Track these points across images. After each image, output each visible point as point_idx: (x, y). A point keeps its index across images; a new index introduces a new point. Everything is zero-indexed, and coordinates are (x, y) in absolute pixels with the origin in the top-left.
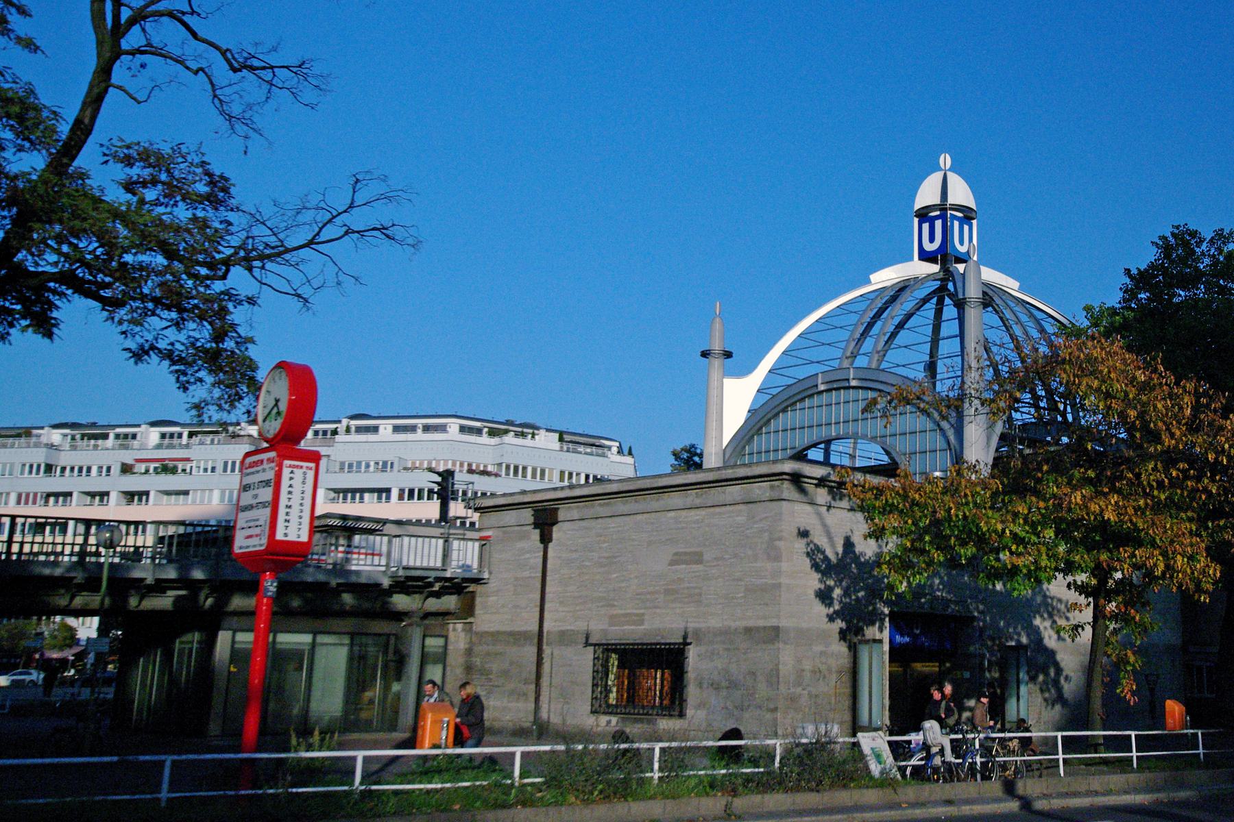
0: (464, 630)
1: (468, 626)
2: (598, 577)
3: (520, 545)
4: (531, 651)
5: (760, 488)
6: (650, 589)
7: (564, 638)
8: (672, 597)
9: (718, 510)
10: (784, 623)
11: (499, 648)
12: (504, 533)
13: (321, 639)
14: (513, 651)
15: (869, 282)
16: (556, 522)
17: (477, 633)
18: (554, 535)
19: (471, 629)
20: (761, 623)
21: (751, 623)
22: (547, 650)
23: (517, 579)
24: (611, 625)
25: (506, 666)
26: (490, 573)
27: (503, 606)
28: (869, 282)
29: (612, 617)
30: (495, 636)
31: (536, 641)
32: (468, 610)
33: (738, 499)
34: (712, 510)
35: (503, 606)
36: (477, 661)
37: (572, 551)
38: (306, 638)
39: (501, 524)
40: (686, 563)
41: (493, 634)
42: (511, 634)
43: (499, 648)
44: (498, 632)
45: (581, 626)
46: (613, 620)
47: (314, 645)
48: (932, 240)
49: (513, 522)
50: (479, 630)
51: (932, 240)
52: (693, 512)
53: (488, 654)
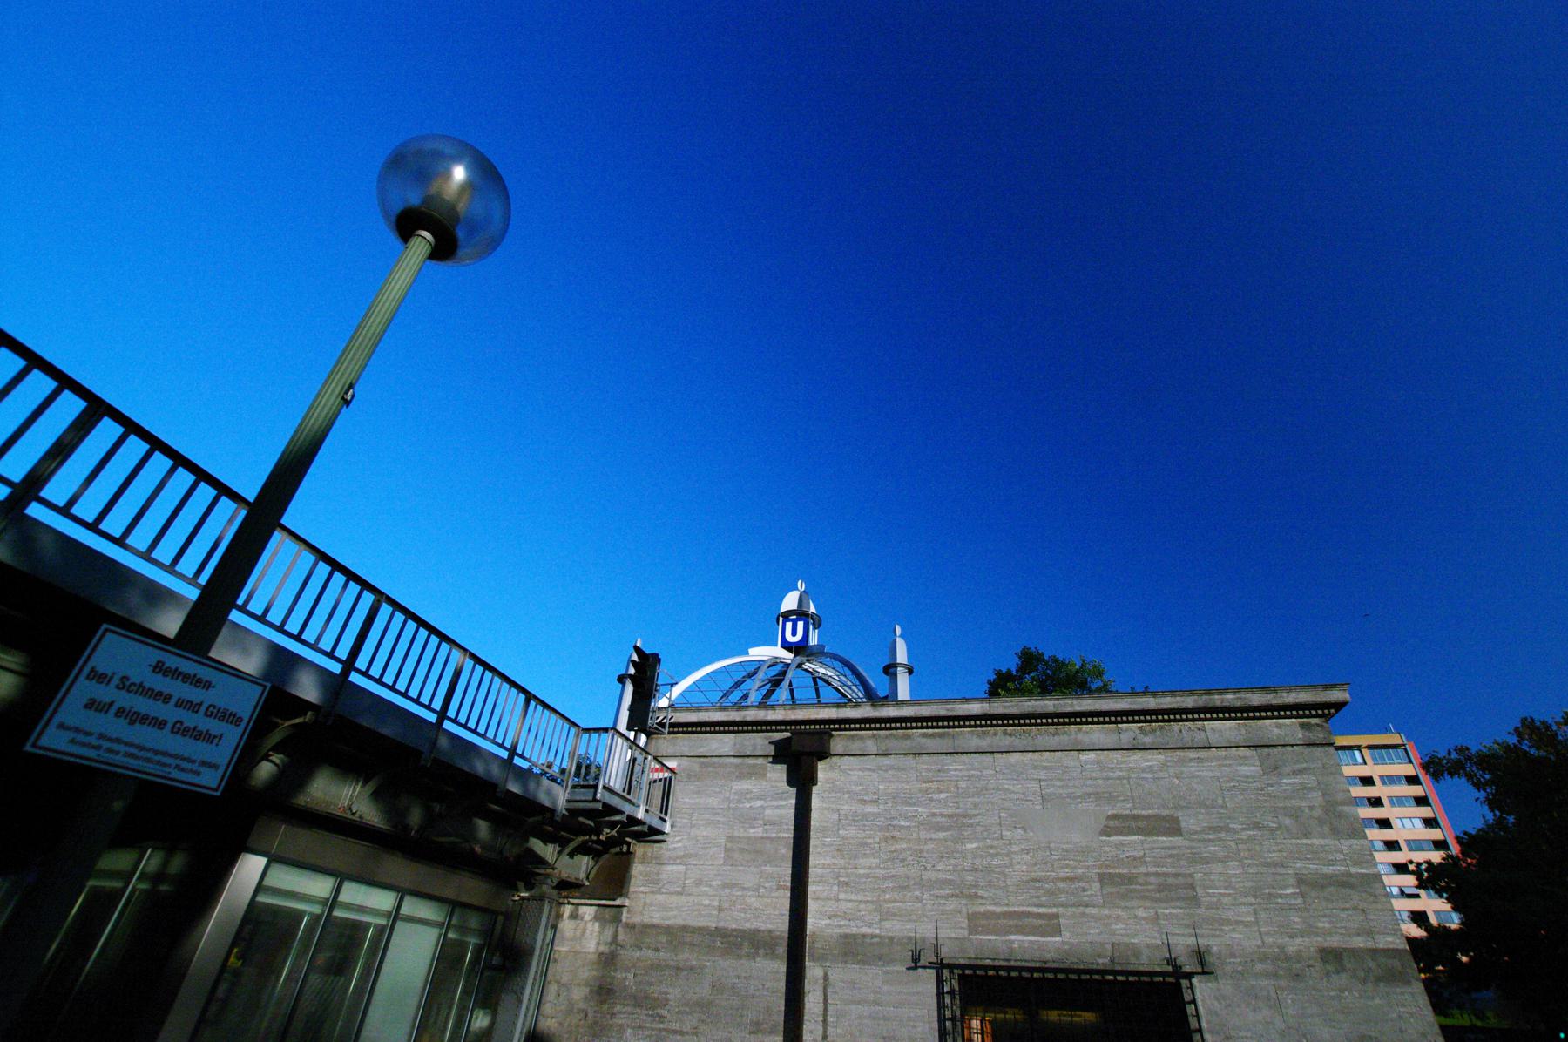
0: (596, 918)
1: (608, 913)
2: (930, 846)
3: (745, 785)
4: (777, 969)
5: (1279, 726)
6: (1066, 872)
7: (852, 949)
8: (1123, 889)
9: (1192, 754)
10: (1213, 943)
11: (686, 956)
12: (703, 765)
13: (411, 907)
14: (727, 968)
15: (747, 653)
16: (824, 754)
17: (631, 927)
18: (821, 775)
19: (617, 920)
20: (1359, 942)
21: (1334, 942)
22: (813, 971)
23: (730, 839)
24: (973, 929)
25: (704, 991)
27: (698, 883)
28: (747, 653)
29: (972, 917)
30: (677, 936)
31: (782, 950)
32: (613, 883)
33: (1239, 740)
34: (1178, 753)
35: (698, 883)
36: (628, 979)
37: (863, 802)
38: (383, 900)
39: (702, 751)
40: (1139, 831)
41: (668, 930)
42: (721, 933)
43: (686, 956)
44: (684, 928)
45: (896, 928)
46: (976, 922)
47: (395, 916)
48: (794, 633)
49: (727, 750)
50: (637, 919)
51: (794, 633)
52: (1137, 756)
53: (656, 967)
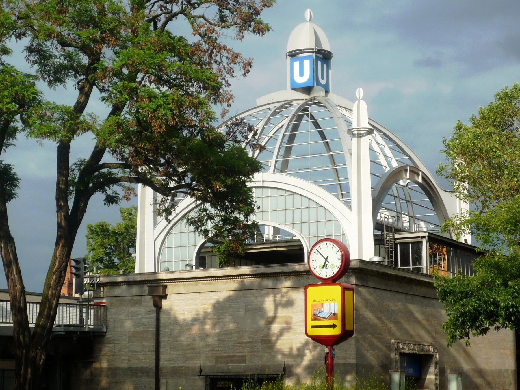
22: (163, 381)
26: (107, 329)
48: (302, 74)
51: (302, 74)
